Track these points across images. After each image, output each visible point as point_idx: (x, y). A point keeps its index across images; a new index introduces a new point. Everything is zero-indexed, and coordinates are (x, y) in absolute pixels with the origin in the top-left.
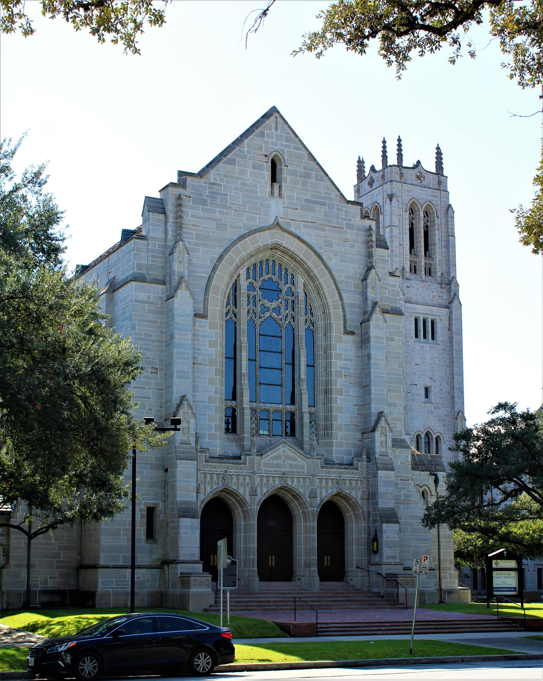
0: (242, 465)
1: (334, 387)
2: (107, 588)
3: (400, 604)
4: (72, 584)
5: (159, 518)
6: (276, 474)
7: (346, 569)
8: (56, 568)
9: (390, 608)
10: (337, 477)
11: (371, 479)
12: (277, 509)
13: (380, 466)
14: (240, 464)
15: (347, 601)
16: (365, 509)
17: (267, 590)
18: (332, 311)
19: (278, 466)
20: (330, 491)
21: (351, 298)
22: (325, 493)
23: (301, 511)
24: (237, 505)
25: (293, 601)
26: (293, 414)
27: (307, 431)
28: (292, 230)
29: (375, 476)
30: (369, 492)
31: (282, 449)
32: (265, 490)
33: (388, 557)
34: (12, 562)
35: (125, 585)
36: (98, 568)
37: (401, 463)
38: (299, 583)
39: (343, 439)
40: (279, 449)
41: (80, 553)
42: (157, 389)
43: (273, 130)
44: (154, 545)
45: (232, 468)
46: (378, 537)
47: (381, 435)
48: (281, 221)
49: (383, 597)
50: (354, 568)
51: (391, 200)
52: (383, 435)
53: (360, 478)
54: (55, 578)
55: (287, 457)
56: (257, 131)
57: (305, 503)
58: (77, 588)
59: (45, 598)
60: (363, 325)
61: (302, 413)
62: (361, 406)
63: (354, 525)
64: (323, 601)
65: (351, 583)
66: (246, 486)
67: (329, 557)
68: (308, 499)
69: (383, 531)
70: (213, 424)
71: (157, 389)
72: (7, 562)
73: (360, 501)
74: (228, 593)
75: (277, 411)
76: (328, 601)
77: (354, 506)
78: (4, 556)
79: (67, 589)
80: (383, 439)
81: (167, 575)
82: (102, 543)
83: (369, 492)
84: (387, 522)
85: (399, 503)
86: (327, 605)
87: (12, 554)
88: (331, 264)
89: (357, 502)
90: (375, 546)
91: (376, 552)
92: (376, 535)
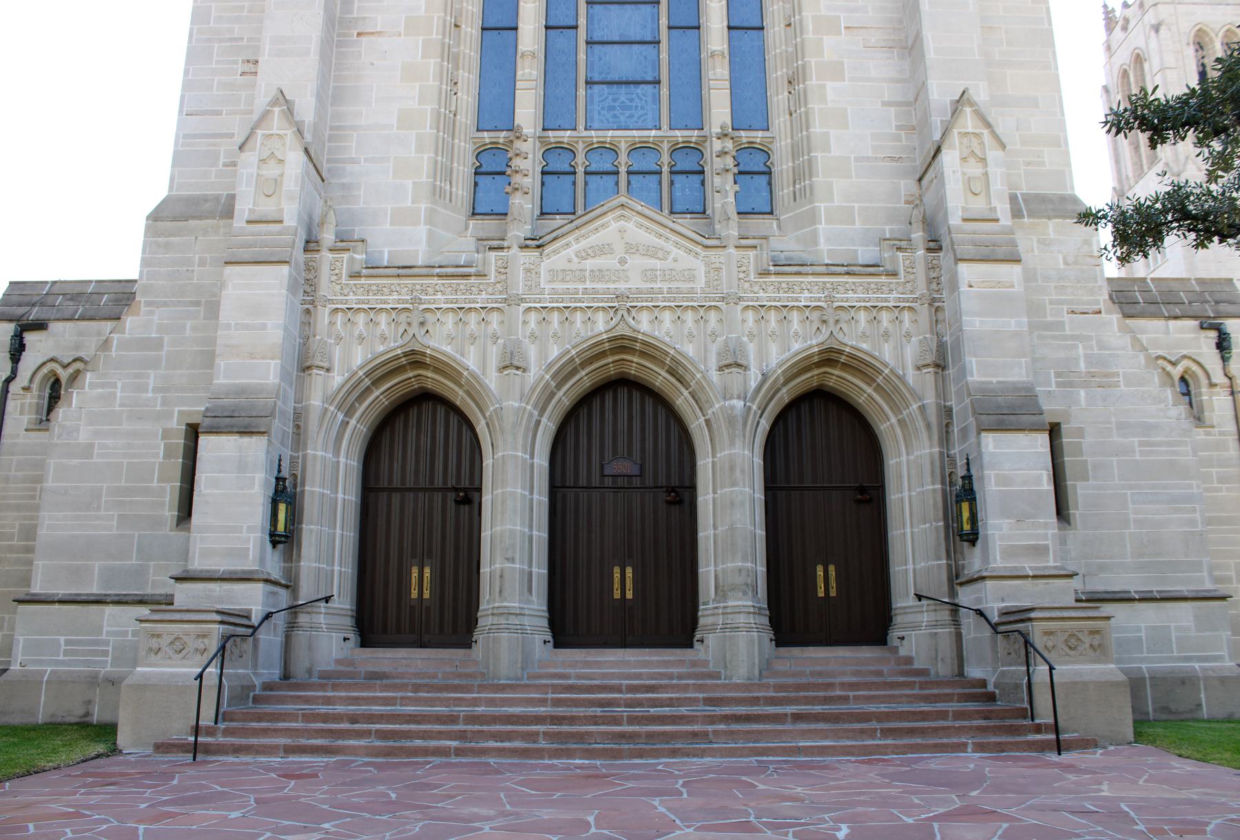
0: (472, 280)
2: (41, 662)
7: (894, 606)
9: (980, 747)
11: (938, 303)
15: (797, 717)
16: (930, 399)
19: (598, 275)
20: (796, 346)
22: (776, 349)
31: (614, 225)
32: (554, 352)
33: (1009, 552)
35: (96, 653)
37: (1066, 263)
45: (441, 294)
47: (964, 159)
51: (1157, 31)
52: (972, 160)
55: (631, 249)
65: (903, 652)
66: (489, 342)
68: (714, 376)
69: (986, 459)
70: (409, 184)
73: (911, 376)
84: (1000, 427)
85: (1070, 384)
90: (966, 514)
92: (968, 478)
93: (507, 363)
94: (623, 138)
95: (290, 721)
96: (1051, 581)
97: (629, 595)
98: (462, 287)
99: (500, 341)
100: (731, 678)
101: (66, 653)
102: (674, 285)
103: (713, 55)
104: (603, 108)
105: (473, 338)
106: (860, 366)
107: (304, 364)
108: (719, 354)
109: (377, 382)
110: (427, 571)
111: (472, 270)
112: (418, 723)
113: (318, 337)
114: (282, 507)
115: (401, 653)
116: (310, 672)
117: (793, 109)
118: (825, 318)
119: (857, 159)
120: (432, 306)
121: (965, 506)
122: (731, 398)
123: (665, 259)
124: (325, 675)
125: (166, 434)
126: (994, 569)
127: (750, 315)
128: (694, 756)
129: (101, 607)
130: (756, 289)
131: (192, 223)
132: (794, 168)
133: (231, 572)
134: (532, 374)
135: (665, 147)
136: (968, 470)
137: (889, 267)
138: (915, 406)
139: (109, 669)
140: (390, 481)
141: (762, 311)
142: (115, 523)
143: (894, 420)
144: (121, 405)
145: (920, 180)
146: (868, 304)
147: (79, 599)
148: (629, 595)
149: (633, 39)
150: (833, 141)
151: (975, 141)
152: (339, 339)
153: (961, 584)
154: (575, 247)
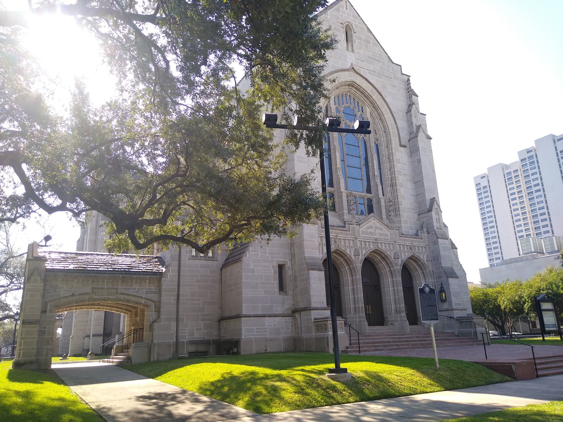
4: (214, 336)
5: (288, 273)
8: (201, 321)
12: (371, 267)
13: (439, 236)
14: (346, 231)
18: (391, 130)
19: (371, 233)
20: (406, 254)
21: (402, 124)
22: (404, 256)
25: (362, 343)
26: (370, 201)
28: (362, 74)
29: (436, 243)
31: (373, 221)
32: (364, 252)
34: (163, 317)
36: (241, 317)
39: (408, 217)
40: (371, 221)
41: (221, 308)
43: (345, 9)
48: (355, 67)
54: (201, 329)
55: (376, 227)
56: (335, 7)
58: (219, 337)
59: (192, 348)
60: (411, 141)
61: (379, 199)
62: (414, 196)
72: (159, 317)
73: (426, 262)
74: (432, 328)
77: (422, 266)
78: (156, 311)
79: (211, 339)
81: (299, 322)
82: (244, 295)
87: (164, 309)
88: (387, 100)
90: (444, 295)
92: (442, 287)
106: (384, 257)
121: (444, 294)
125: (273, 267)
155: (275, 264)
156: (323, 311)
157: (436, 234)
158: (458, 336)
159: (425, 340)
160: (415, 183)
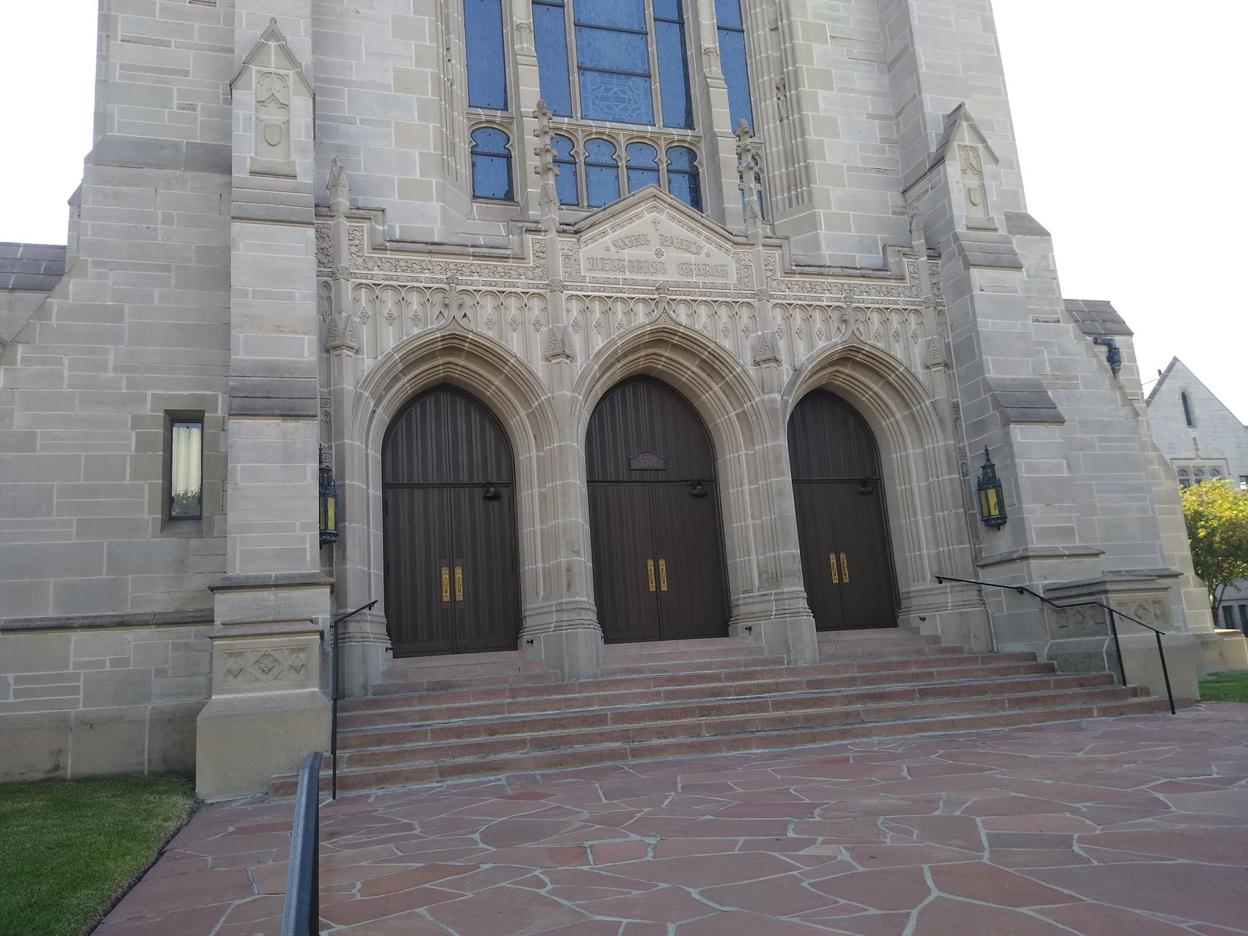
0: (511, 263)
1: (804, 67)
3: (1135, 692)
6: (634, 291)
7: (902, 590)
10: (839, 300)
13: (972, 256)
16: (941, 396)
17: (627, 671)
19: (637, 265)
20: (821, 344)
22: (805, 349)
23: (733, 414)
24: (515, 401)
27: (730, 182)
29: (963, 288)
30: (947, 345)
31: (648, 216)
32: (599, 343)
33: (1044, 533)
38: (750, 641)
39: (847, 197)
42: (212, 48)
44: (194, 543)
45: (478, 276)
46: (999, 474)
47: (964, 171)
49: (1050, 669)
50: (929, 583)
52: (969, 172)
53: (913, 303)
55: (667, 241)
57: (741, 383)
62: (889, 118)
63: (910, 452)
64: (829, 701)
65: (925, 629)
67: (843, 556)
68: (751, 370)
69: (1016, 449)
71: (212, 48)
73: (920, 372)
75: (637, 143)
76: (850, 700)
77: (904, 390)
80: (973, 182)
83: (947, 345)
86: (848, 715)
89: (913, 375)
90: (993, 500)
91: (996, 523)
92: (989, 467)
93: (559, 350)
94: (623, 131)
95: (418, 740)
96: (1082, 559)
97: (664, 588)
98: (500, 269)
99: (543, 329)
100: (796, 663)
101: (17, 694)
102: (709, 280)
103: (519, 27)
104: (597, 98)
105: (514, 324)
107: (332, 344)
108: (752, 349)
109: (408, 368)
110: (458, 572)
111: (509, 252)
112: (564, 727)
113: (344, 314)
114: (331, 501)
115: (452, 659)
116: (365, 687)
117: (784, 115)
118: (846, 317)
119: (849, 169)
120: (470, 288)
121: (992, 493)
122: (771, 391)
123: (698, 253)
124: (379, 690)
125: (137, 422)
126: (1034, 550)
127: (574, 305)
128: (863, 736)
129: (63, 634)
130: (370, 265)
131: (149, 172)
132: (788, 175)
133: (286, 577)
134: (579, 364)
135: (663, 144)
136: (988, 460)
137: (517, 250)
138: (928, 402)
139: (81, 709)
140: (411, 475)
141: (377, 290)
142: (74, 530)
143: (523, 414)
144: (70, 386)
145: (904, 192)
146: (881, 306)
147: (32, 625)
148: (664, 588)
149: (620, 27)
150: (827, 151)
151: (277, 85)
152: (364, 316)
153: (982, 566)
154: (612, 236)
155: (147, 409)
156: (284, 593)
157: (961, 250)
158: (1050, 669)
159: (816, 702)
160: (890, 66)
